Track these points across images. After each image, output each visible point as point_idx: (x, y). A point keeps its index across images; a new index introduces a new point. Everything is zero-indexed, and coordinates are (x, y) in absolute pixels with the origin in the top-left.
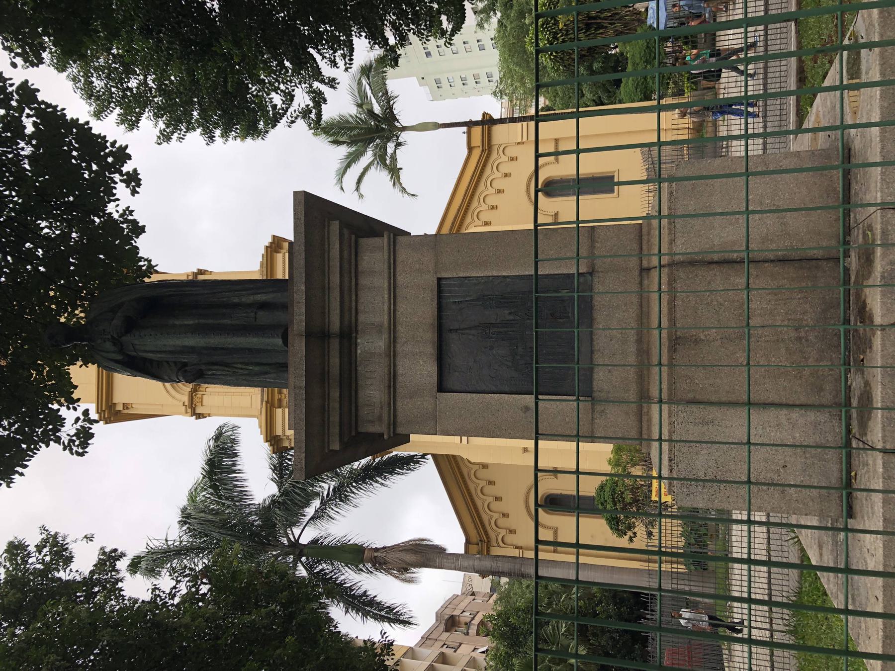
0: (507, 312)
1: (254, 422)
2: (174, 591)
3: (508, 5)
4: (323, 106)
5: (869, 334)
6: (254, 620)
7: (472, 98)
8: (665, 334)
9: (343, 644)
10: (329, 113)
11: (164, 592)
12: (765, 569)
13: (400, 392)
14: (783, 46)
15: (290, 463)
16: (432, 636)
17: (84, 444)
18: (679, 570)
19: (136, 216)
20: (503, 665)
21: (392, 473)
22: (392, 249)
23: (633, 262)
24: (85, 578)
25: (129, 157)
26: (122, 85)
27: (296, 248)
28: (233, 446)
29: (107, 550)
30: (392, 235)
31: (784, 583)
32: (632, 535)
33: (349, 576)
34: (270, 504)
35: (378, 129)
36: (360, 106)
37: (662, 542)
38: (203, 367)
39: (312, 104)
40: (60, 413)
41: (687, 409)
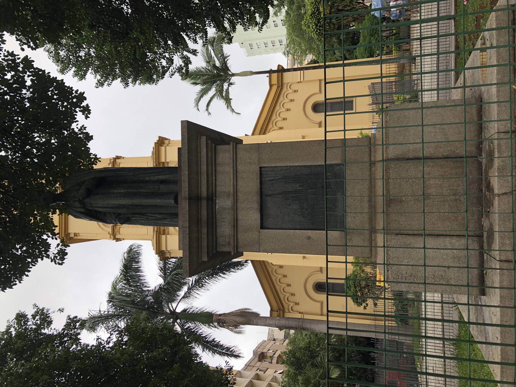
0: (298, 185)
1: (150, 243)
2: (109, 339)
3: (291, 3)
4: (190, 65)
5: (492, 198)
6: (155, 355)
7: (271, 54)
8: (405, 341)
9: (204, 368)
10: (192, 67)
11: (103, 340)
12: (440, 323)
13: (240, 229)
14: (447, 31)
15: (170, 266)
16: (251, 364)
17: (62, 259)
18: (393, 325)
19: (87, 130)
20: (292, 380)
21: (229, 271)
22: (235, 152)
23: (366, 159)
24: (59, 333)
25: (85, 99)
26: (76, 55)
27: (183, 151)
28: (138, 257)
29: (72, 317)
30: (234, 144)
31: (451, 331)
32: (366, 305)
33: (205, 330)
34: (158, 290)
35: (218, 75)
36: (207, 62)
37: (386, 309)
38: (130, 216)
39: (183, 65)
40: (47, 241)
41: (396, 238)
